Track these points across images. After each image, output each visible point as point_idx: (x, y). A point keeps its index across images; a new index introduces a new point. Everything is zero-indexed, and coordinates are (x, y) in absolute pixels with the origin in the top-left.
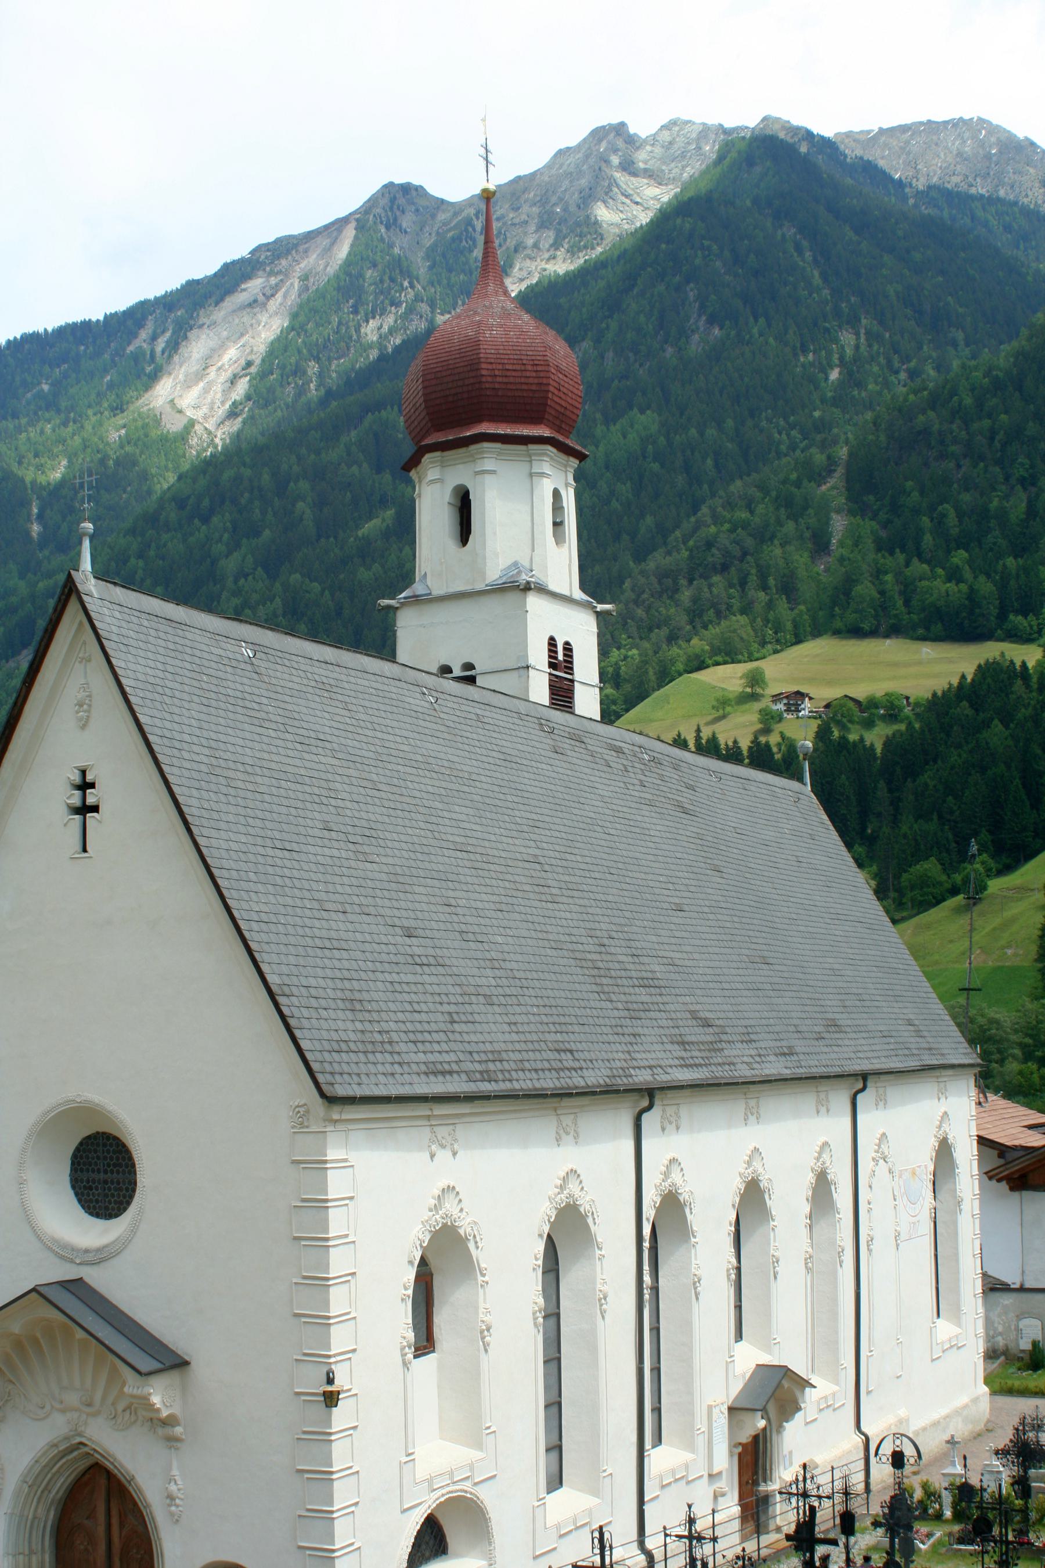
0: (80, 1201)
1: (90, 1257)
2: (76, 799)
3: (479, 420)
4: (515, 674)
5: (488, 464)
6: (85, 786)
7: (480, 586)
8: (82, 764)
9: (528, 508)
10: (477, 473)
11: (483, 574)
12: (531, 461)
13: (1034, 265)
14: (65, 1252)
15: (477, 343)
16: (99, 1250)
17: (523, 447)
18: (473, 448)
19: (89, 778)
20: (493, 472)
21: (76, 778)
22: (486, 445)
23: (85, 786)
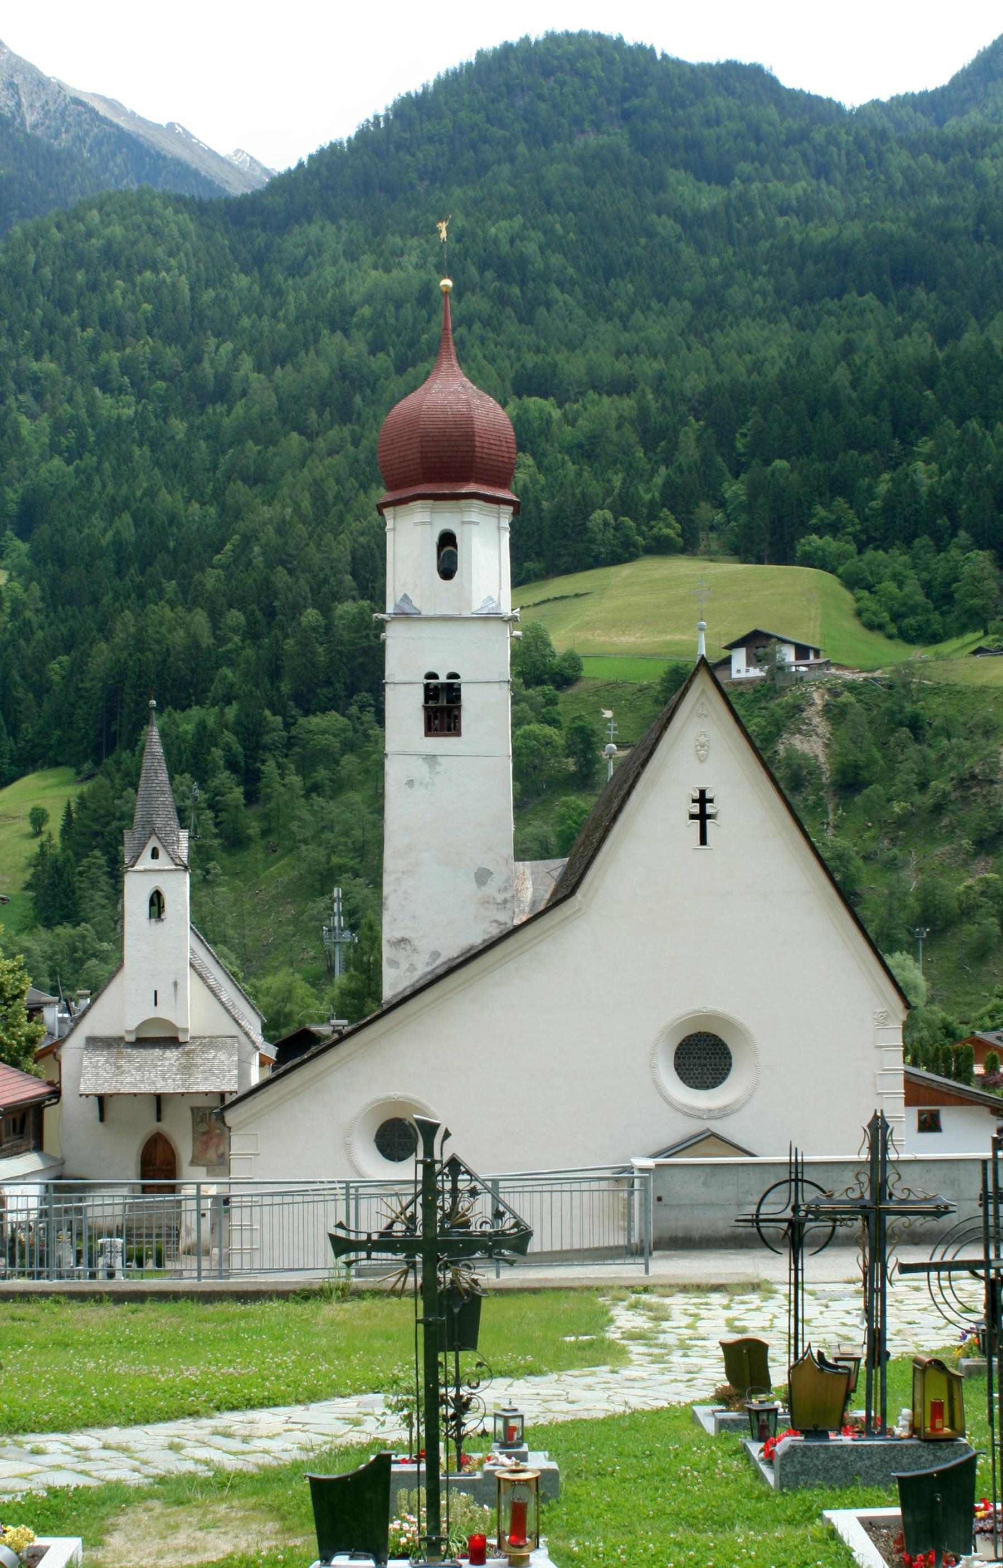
0: (681, 1078)
1: (716, 1114)
2: (696, 809)
3: (467, 479)
4: (497, 686)
5: (474, 517)
6: (703, 800)
7: (466, 614)
8: (702, 786)
9: (497, 554)
10: (463, 523)
11: (469, 604)
12: (499, 518)
13: (81, 245)
14: (691, 1113)
15: (470, 419)
16: (720, 1109)
17: (496, 506)
18: (463, 502)
19: (708, 796)
20: (477, 523)
21: (697, 795)
22: (475, 501)
23: (703, 800)
